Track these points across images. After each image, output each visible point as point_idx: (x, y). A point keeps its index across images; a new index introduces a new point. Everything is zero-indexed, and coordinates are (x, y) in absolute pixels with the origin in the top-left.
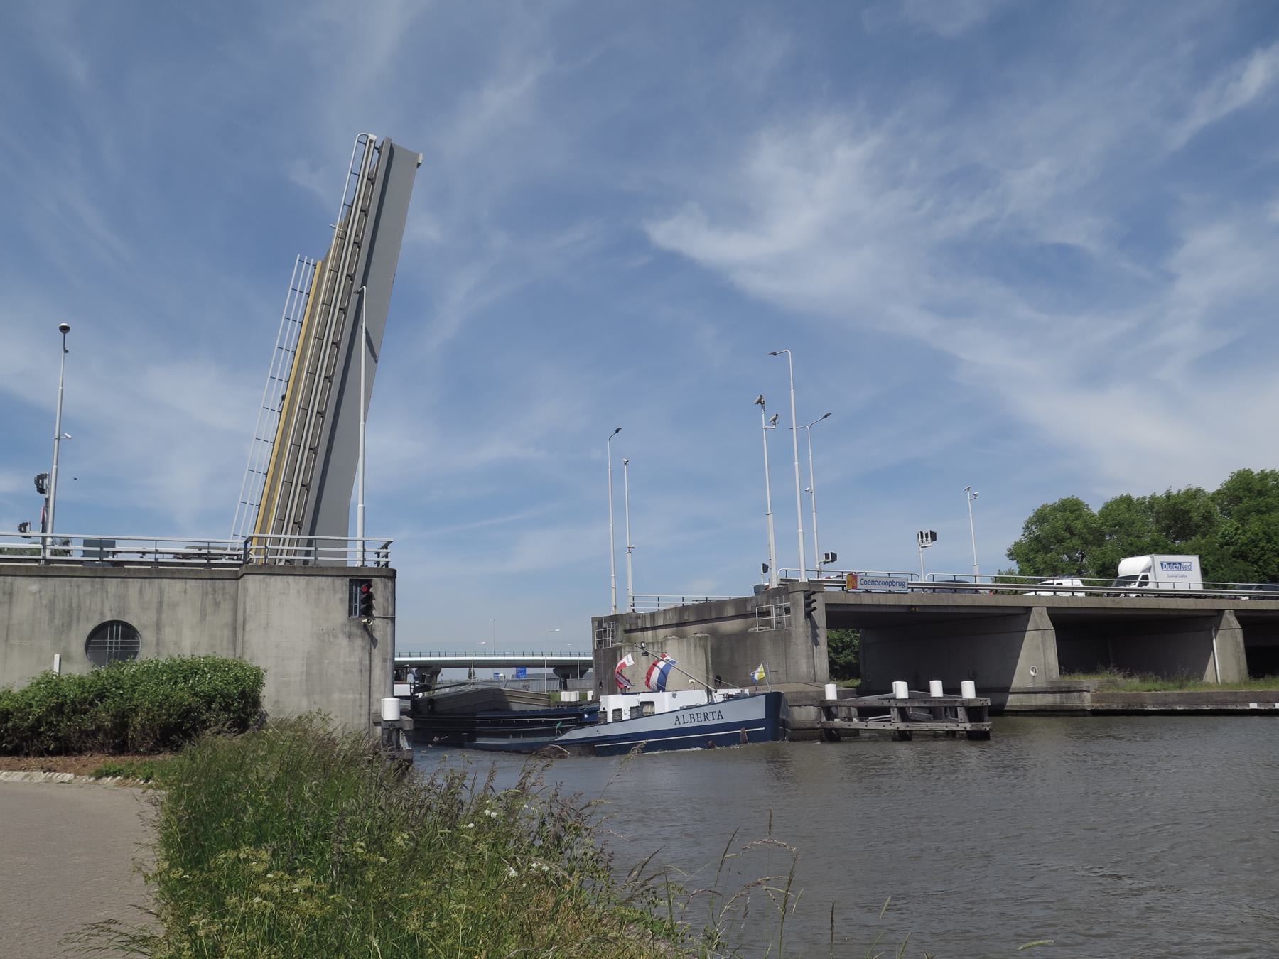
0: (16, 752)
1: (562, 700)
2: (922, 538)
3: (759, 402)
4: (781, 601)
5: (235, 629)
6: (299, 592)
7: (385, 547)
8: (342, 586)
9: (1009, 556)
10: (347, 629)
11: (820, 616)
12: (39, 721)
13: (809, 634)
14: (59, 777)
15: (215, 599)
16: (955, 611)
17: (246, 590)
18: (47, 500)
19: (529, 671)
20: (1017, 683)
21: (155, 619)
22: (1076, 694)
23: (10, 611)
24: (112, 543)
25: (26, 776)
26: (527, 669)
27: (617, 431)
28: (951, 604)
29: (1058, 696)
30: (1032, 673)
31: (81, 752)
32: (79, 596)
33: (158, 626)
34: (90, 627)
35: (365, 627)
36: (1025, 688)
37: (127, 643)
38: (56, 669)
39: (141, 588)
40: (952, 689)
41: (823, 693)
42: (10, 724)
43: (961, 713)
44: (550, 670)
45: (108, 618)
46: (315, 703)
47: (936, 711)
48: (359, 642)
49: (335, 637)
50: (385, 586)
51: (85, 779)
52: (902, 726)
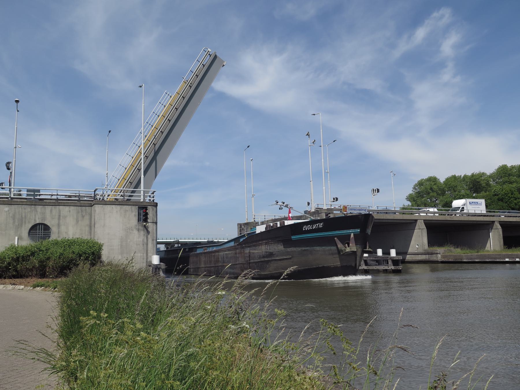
15: (82, 215)
24: (39, 191)
33: (59, 225)
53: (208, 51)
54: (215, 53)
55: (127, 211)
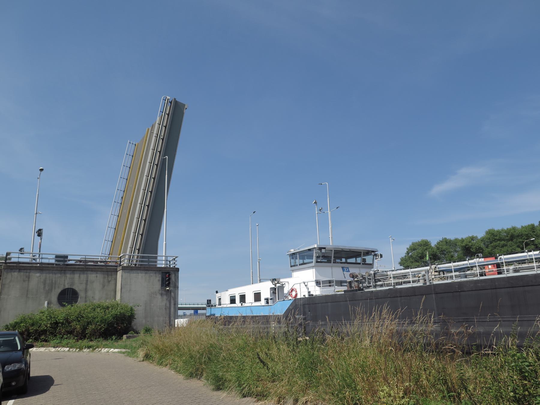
15: (108, 280)
19: (199, 311)
24: (67, 257)
26: (198, 311)
27: (254, 212)
33: (86, 290)
34: (59, 291)
46: (148, 321)
53: (168, 99)
54: (175, 99)
55: (152, 276)
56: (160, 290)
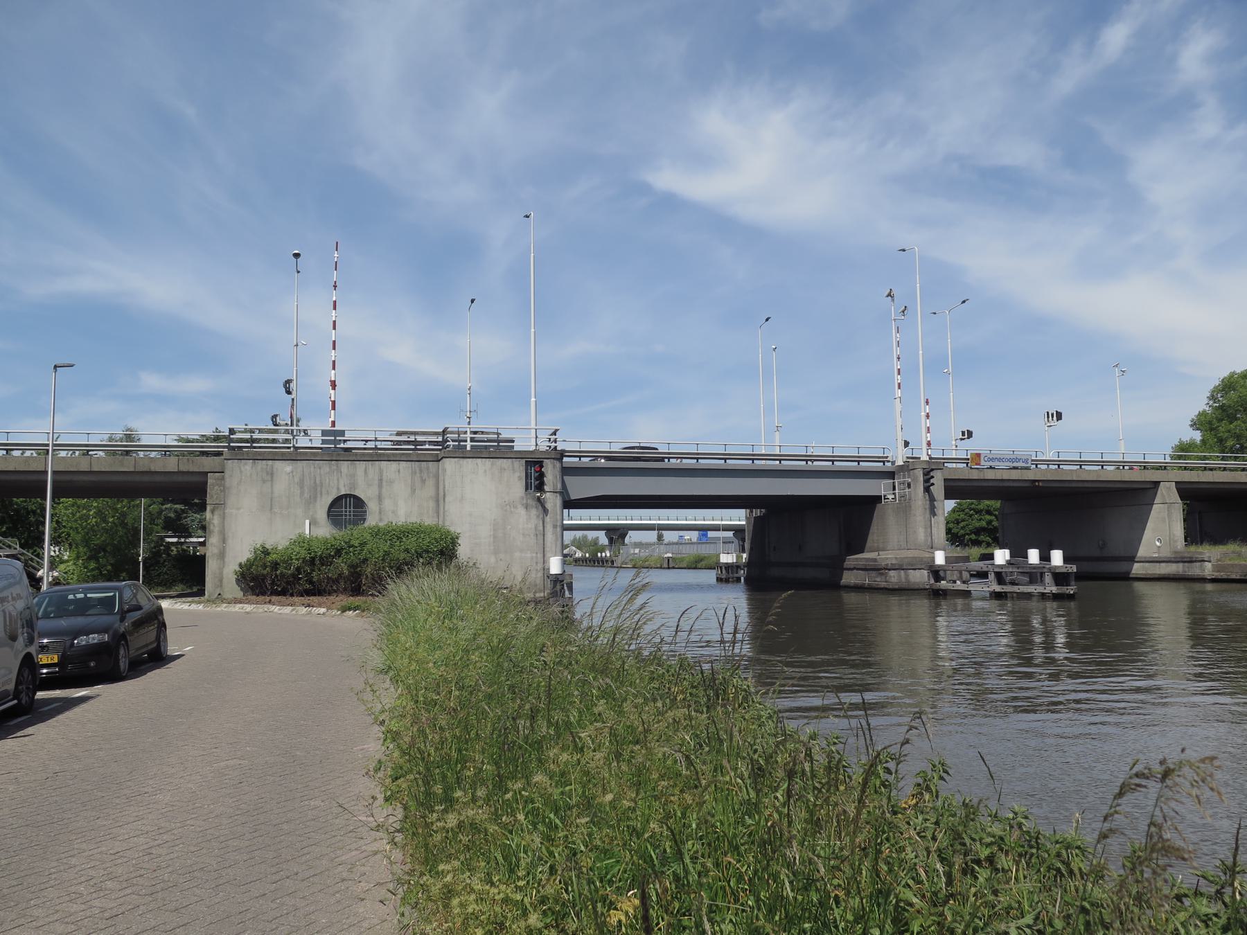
0: (283, 593)
1: (721, 561)
2: (1048, 417)
3: (889, 295)
4: (904, 477)
5: (437, 501)
6: (485, 471)
7: (554, 433)
8: (519, 466)
9: (1191, 426)
10: (525, 502)
11: (938, 489)
12: (298, 569)
13: (928, 506)
14: (316, 610)
15: (421, 477)
16: (1080, 485)
17: (445, 470)
18: (293, 399)
19: (711, 534)
20: (1142, 552)
21: (377, 493)
22: (1198, 564)
23: (272, 486)
25: (293, 610)
26: (709, 532)
27: (767, 320)
28: (1075, 479)
29: (1181, 565)
30: (1158, 544)
31: (330, 594)
32: (320, 475)
33: (380, 498)
34: (330, 500)
35: (539, 499)
36: (1150, 557)
37: (357, 512)
38: (307, 532)
39: (366, 470)
40: (1045, 557)
41: (933, 559)
42: (278, 572)
43: (1048, 578)
44: (730, 534)
45: (343, 493)
47: (1034, 576)
48: (534, 512)
49: (515, 507)
50: (554, 467)
51: (335, 612)
52: (998, 588)
56: (523, 498)
